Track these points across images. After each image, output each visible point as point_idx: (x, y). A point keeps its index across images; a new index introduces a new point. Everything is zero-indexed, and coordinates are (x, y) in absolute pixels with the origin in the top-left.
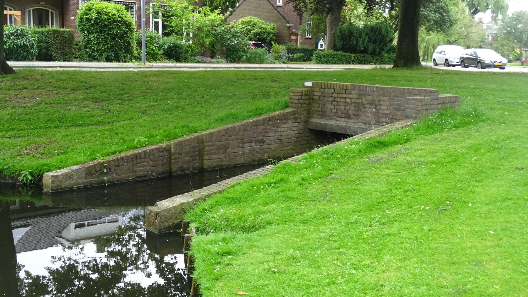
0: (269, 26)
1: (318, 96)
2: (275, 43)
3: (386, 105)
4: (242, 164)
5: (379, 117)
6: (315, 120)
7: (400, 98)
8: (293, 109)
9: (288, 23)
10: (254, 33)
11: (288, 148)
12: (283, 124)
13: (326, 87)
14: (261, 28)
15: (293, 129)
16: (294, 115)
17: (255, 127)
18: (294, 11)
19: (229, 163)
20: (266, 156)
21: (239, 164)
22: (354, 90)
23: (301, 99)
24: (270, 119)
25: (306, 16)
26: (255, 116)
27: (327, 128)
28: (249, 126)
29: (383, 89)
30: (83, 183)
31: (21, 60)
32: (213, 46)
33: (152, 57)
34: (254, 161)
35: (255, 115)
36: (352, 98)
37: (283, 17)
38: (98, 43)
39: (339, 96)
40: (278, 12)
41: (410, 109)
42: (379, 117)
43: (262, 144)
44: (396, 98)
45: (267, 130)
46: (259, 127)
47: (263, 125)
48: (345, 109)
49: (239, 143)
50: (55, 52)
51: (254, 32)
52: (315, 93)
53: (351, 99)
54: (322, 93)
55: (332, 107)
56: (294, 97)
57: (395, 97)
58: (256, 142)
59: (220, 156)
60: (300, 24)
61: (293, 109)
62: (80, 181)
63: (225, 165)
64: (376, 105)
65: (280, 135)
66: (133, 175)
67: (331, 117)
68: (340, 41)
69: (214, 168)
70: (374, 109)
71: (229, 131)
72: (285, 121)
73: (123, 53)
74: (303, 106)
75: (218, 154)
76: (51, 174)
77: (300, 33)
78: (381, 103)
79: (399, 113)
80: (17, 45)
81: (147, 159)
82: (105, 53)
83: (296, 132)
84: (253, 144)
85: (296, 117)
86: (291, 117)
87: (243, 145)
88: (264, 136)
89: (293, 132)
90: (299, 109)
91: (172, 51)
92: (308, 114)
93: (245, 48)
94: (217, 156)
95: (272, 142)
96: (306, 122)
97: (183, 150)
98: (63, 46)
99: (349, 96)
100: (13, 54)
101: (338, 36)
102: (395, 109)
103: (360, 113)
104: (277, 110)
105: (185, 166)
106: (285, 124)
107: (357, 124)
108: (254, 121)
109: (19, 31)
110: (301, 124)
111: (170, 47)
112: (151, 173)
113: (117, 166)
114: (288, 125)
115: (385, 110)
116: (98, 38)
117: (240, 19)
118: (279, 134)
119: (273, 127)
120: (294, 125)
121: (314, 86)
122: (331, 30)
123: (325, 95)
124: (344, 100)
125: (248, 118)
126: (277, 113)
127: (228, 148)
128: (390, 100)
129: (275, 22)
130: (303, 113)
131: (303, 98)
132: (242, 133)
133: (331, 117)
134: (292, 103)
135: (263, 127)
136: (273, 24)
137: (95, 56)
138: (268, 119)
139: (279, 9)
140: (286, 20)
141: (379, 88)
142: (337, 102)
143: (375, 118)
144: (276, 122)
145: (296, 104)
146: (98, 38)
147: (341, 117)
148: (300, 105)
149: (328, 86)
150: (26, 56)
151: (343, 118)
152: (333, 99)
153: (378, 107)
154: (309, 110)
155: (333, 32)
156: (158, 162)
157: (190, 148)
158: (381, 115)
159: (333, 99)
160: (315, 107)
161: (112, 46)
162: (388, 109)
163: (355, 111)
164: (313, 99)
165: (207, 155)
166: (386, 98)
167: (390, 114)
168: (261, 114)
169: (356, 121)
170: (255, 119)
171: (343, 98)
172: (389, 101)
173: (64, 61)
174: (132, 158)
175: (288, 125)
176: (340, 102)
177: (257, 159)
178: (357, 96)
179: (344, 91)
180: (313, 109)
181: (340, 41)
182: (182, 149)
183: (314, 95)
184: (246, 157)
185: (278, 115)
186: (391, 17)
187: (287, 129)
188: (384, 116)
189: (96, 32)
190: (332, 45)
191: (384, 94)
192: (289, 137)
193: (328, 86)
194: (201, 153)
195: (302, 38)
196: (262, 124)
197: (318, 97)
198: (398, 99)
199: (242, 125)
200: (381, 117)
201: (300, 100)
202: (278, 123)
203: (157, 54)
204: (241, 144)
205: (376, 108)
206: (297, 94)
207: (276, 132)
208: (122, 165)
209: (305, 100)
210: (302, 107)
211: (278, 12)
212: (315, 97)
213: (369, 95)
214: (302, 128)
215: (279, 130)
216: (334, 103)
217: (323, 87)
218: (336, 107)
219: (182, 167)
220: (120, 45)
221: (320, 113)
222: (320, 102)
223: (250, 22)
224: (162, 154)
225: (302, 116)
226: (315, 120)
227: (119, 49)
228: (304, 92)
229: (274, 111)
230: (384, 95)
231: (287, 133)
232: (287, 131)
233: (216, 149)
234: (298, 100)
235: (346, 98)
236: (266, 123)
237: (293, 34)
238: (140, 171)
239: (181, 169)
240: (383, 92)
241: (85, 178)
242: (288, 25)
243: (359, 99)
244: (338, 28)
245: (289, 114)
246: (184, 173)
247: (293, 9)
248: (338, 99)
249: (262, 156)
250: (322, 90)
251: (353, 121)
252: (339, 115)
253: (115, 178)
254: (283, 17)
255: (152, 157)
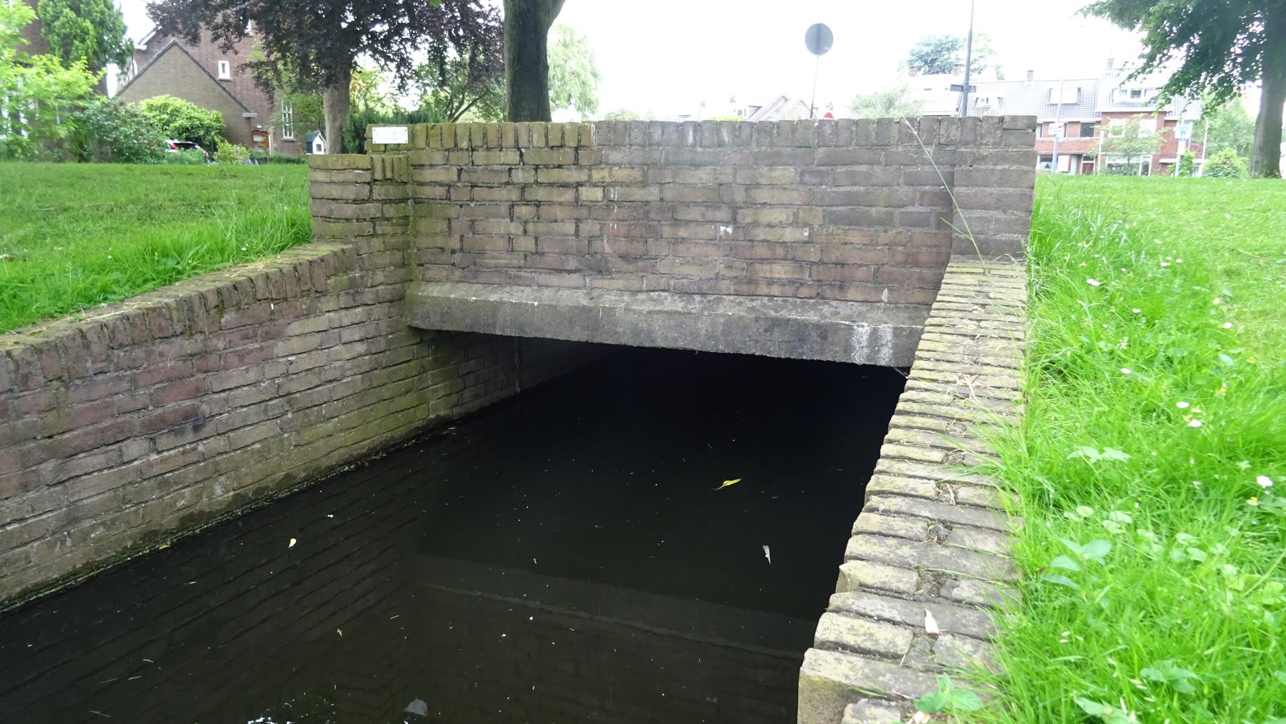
0: (208, 116)
1: (441, 185)
2: (222, 141)
3: (786, 206)
4: (65, 578)
5: (751, 261)
6: (435, 291)
7: (863, 168)
8: (337, 247)
9: (246, 110)
10: (176, 128)
11: (330, 425)
12: (297, 317)
13: (477, 142)
14: (191, 118)
15: (347, 335)
17: (138, 353)
18: (256, 86)
20: (218, 490)
21: (54, 583)
22: (616, 146)
23: (370, 200)
24: (224, 299)
25: (281, 96)
26: (135, 285)
27: (500, 321)
28: (95, 348)
29: (770, 134)
32: (81, 146)
34: (151, 535)
35: (137, 284)
36: (614, 184)
37: (235, 99)
39: (542, 177)
40: (224, 89)
41: (986, 207)
42: (751, 261)
43: (190, 437)
44: (840, 169)
45: (213, 360)
46: (161, 347)
47: (189, 331)
48: (577, 234)
49: (26, 462)
51: (177, 124)
52: (428, 175)
53: (605, 186)
54: (460, 171)
55: (515, 228)
56: (336, 192)
57: (832, 163)
58: (152, 430)
60: (271, 110)
61: (337, 247)
64: (735, 209)
65: (287, 375)
67: (512, 272)
68: (354, 141)
70: (726, 224)
72: (303, 304)
74: (379, 231)
77: (271, 130)
78: (763, 195)
79: (856, 237)
83: (361, 348)
84: (134, 448)
86: (331, 281)
87: (60, 469)
88: (199, 392)
90: (363, 243)
92: (403, 265)
93: (155, 147)
95: (246, 416)
96: (398, 300)
99: (597, 176)
101: (348, 131)
102: (835, 220)
103: (653, 247)
104: (258, 253)
106: (307, 316)
107: (641, 296)
108: (126, 318)
110: (379, 311)
114: (322, 322)
115: (782, 225)
117: (143, 99)
118: (282, 369)
119: (245, 337)
120: (347, 317)
121: (421, 142)
122: (334, 120)
123: (474, 178)
124: (569, 195)
125: (89, 300)
126: (259, 266)
128: (807, 178)
129: (219, 108)
130: (380, 260)
131: (375, 196)
132: (45, 399)
133: (512, 272)
134: (327, 218)
135: (189, 345)
136: (215, 112)
138: (213, 300)
139: (224, 85)
140: (240, 104)
141: (747, 131)
142: (538, 204)
143: (729, 267)
144: (260, 310)
145: (347, 220)
147: (560, 271)
148: (367, 227)
149: (485, 136)
151: (570, 272)
152: (515, 195)
153: (746, 216)
154: (404, 248)
155: (338, 124)
158: (761, 251)
159: (515, 195)
160: (430, 233)
162: (795, 223)
163: (631, 238)
164: (417, 201)
166: (785, 173)
167: (808, 242)
168: (170, 278)
169: (635, 284)
170: (130, 307)
171: (565, 185)
172: (802, 183)
175: (322, 322)
176: (551, 203)
177: (169, 521)
178: (636, 174)
179: (567, 156)
180: (423, 242)
181: (354, 141)
183: (421, 184)
184: (93, 528)
185: (267, 277)
186: (438, 102)
187: (316, 340)
188: (780, 252)
190: (338, 147)
191: (778, 154)
193: (485, 136)
195: (275, 139)
196: (179, 328)
197: (440, 192)
198: (851, 175)
199: (37, 350)
200: (762, 260)
201: (363, 201)
202: (272, 317)
204: (49, 466)
205: (734, 221)
206: (350, 176)
209: (384, 202)
210: (374, 235)
211: (224, 89)
212: (427, 192)
213: (696, 165)
214: (383, 326)
215: (280, 347)
216: (523, 211)
217: (465, 145)
218: (530, 227)
221: (457, 258)
222: (453, 211)
223: (166, 106)
225: (380, 277)
226: (435, 291)
228: (378, 166)
229: (244, 257)
230: (774, 160)
231: (318, 359)
234: (355, 201)
235: (579, 184)
236: (202, 323)
237: (257, 132)
240: (772, 145)
242: (246, 115)
243: (644, 184)
244: (348, 116)
245: (318, 271)
247: (251, 84)
248: (541, 194)
250: (461, 158)
251: (620, 283)
252: (550, 260)
254: (235, 99)
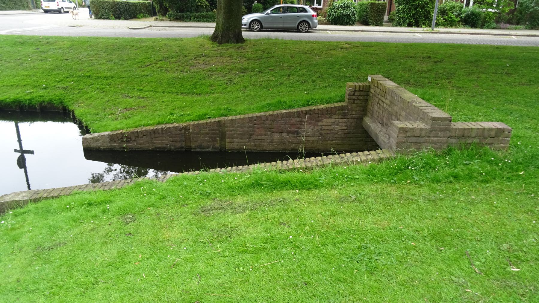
4: (269, 150)
12: (326, 118)
15: (340, 124)
16: (343, 110)
17: (287, 119)
19: (255, 148)
23: (354, 95)
30: (108, 146)
31: (344, 25)
33: (450, 23)
34: (285, 149)
38: (404, 12)
47: (298, 117)
50: (370, 19)
58: (288, 132)
59: (244, 141)
62: (105, 144)
63: (250, 149)
65: (321, 129)
66: (152, 146)
69: (235, 150)
71: (253, 120)
72: (328, 116)
73: (423, 20)
75: (241, 138)
76: (400, 124)
80: (343, 14)
81: (164, 135)
82: (408, 20)
83: (345, 128)
84: (284, 134)
85: (344, 113)
87: (271, 134)
88: (299, 128)
89: (339, 128)
91: (469, 18)
94: (240, 140)
97: (202, 132)
98: (377, 14)
100: (339, 20)
105: (204, 144)
109: (345, 4)
111: (467, 15)
112: (170, 146)
113: (137, 137)
114: (333, 120)
116: (404, 8)
120: (341, 120)
127: (254, 135)
132: (270, 123)
135: (298, 119)
137: (401, 22)
138: (304, 112)
146: (404, 8)
150: (348, 22)
156: (175, 139)
157: (209, 130)
161: (414, 15)
165: (229, 138)
173: (376, 25)
174: (150, 133)
175: (333, 120)
177: (289, 148)
182: (200, 130)
187: (331, 124)
189: (404, 4)
192: (333, 132)
194: (223, 136)
203: (455, 21)
207: (316, 125)
208: (142, 137)
209: (359, 96)
210: (354, 103)
214: (353, 124)
215: (320, 123)
219: (202, 145)
220: (421, 14)
224: (179, 132)
227: (419, 17)
231: (331, 128)
232: (332, 125)
233: (239, 134)
238: (160, 143)
239: (200, 147)
241: (109, 142)
246: (203, 150)
249: (296, 146)
253: (136, 146)
255: (170, 133)
